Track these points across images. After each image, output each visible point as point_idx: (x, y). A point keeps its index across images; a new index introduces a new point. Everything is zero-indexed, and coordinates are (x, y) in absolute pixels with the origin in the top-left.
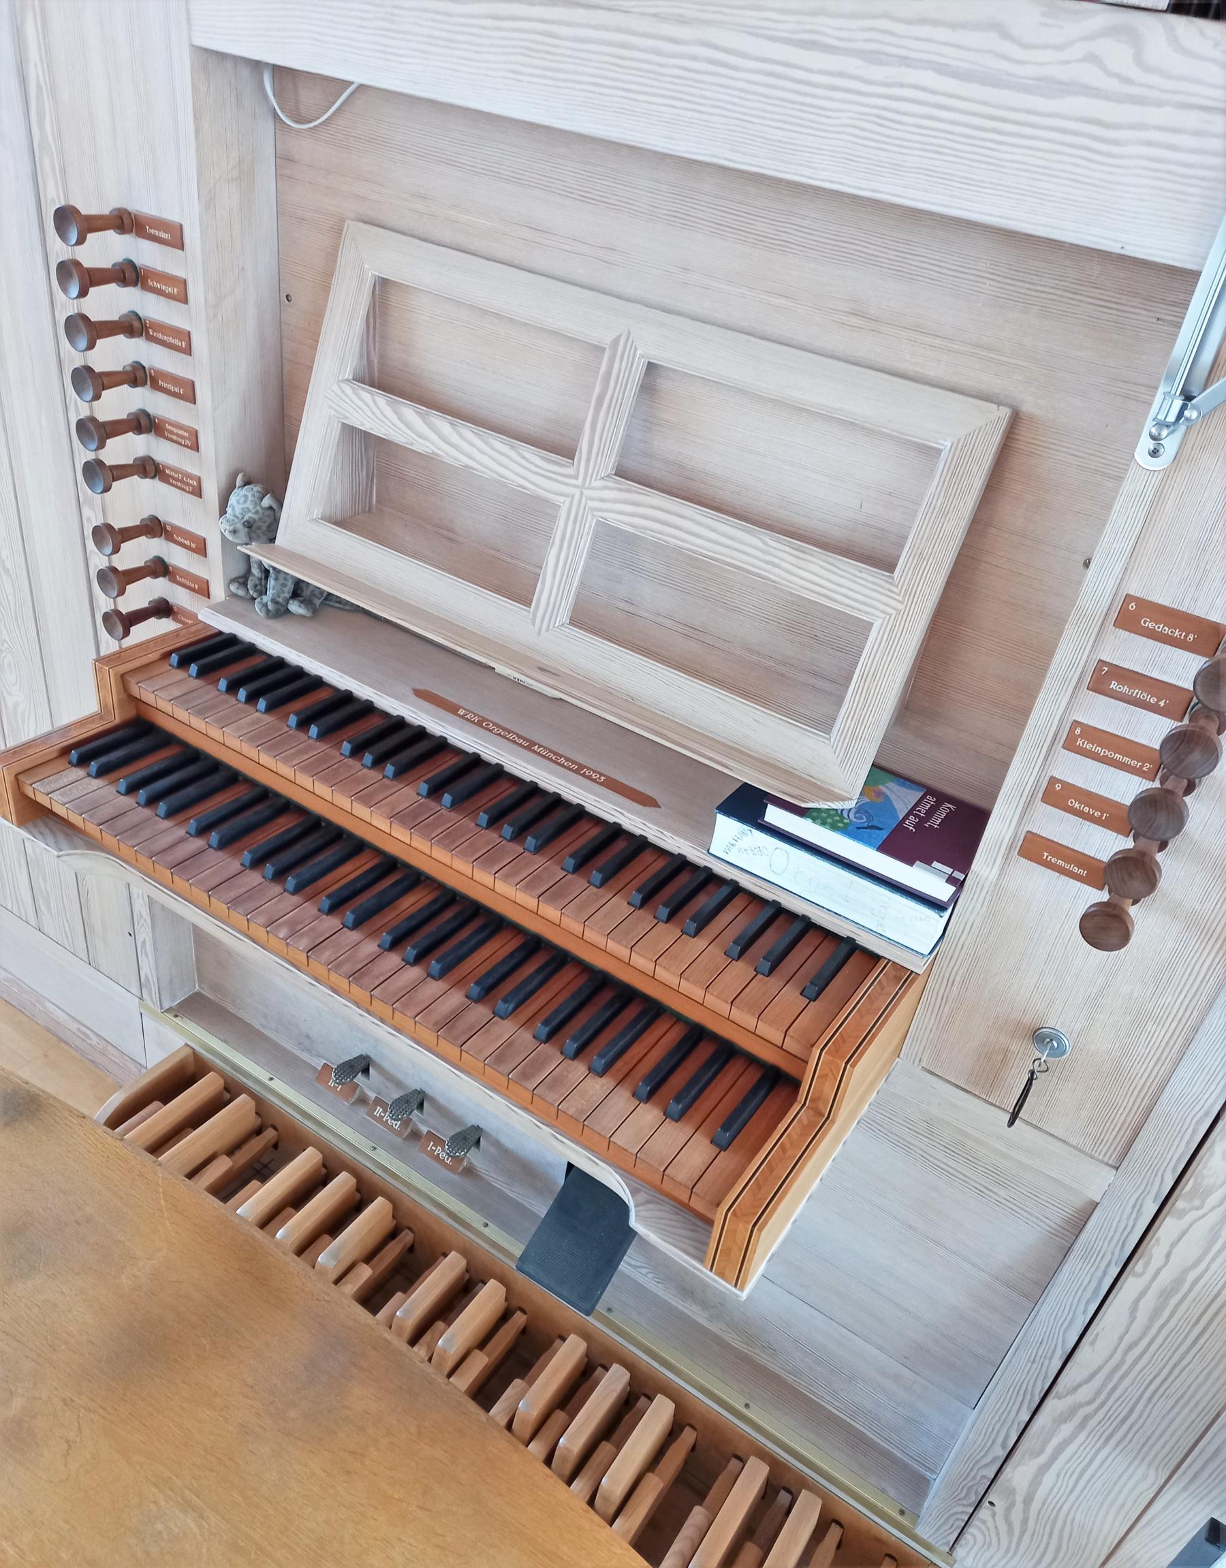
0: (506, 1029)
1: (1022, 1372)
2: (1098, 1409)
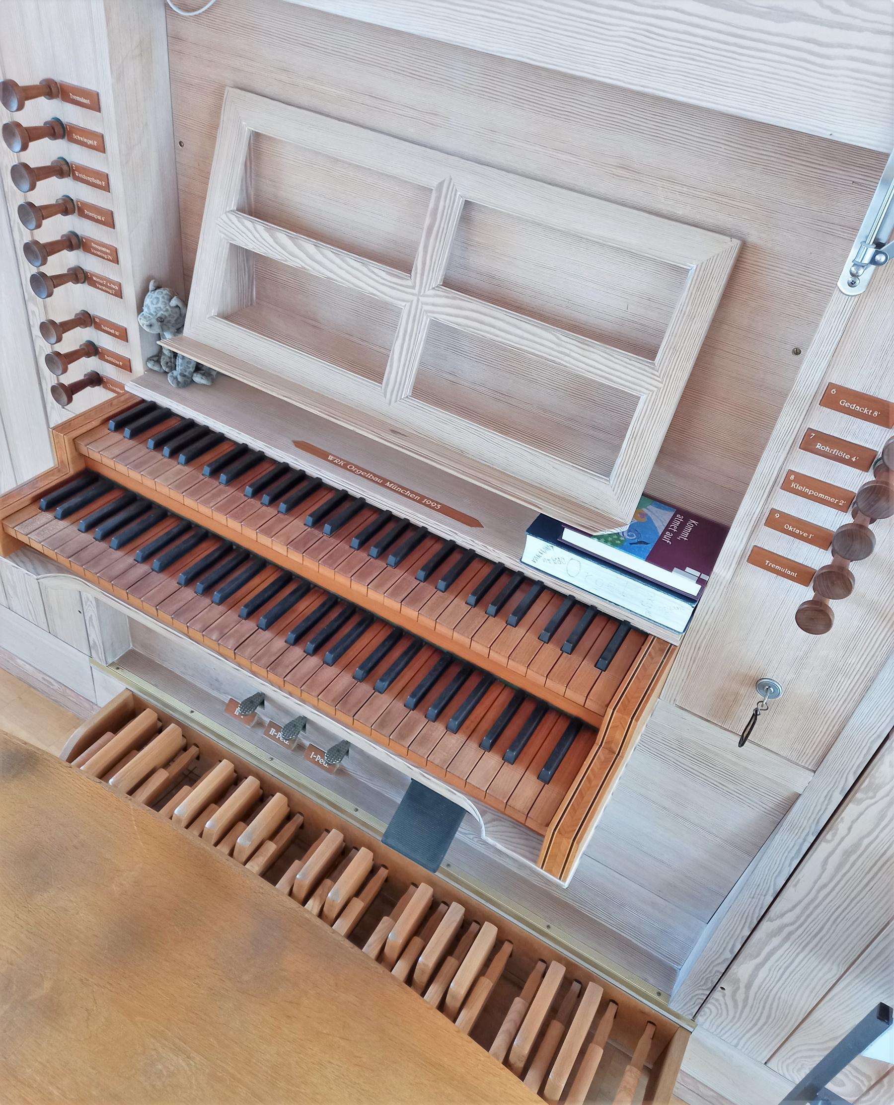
0: (384, 701)
1: (743, 902)
2: (797, 929)
